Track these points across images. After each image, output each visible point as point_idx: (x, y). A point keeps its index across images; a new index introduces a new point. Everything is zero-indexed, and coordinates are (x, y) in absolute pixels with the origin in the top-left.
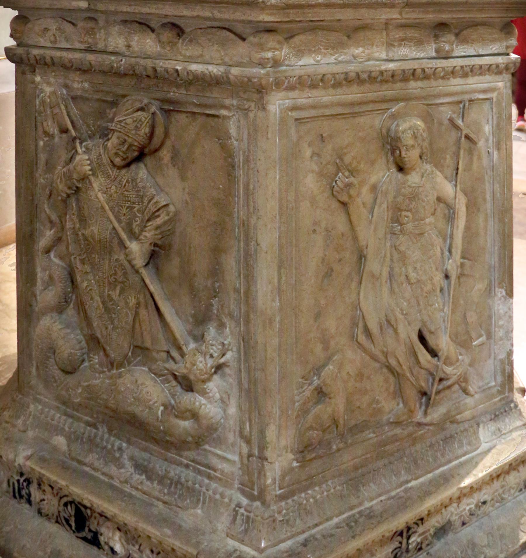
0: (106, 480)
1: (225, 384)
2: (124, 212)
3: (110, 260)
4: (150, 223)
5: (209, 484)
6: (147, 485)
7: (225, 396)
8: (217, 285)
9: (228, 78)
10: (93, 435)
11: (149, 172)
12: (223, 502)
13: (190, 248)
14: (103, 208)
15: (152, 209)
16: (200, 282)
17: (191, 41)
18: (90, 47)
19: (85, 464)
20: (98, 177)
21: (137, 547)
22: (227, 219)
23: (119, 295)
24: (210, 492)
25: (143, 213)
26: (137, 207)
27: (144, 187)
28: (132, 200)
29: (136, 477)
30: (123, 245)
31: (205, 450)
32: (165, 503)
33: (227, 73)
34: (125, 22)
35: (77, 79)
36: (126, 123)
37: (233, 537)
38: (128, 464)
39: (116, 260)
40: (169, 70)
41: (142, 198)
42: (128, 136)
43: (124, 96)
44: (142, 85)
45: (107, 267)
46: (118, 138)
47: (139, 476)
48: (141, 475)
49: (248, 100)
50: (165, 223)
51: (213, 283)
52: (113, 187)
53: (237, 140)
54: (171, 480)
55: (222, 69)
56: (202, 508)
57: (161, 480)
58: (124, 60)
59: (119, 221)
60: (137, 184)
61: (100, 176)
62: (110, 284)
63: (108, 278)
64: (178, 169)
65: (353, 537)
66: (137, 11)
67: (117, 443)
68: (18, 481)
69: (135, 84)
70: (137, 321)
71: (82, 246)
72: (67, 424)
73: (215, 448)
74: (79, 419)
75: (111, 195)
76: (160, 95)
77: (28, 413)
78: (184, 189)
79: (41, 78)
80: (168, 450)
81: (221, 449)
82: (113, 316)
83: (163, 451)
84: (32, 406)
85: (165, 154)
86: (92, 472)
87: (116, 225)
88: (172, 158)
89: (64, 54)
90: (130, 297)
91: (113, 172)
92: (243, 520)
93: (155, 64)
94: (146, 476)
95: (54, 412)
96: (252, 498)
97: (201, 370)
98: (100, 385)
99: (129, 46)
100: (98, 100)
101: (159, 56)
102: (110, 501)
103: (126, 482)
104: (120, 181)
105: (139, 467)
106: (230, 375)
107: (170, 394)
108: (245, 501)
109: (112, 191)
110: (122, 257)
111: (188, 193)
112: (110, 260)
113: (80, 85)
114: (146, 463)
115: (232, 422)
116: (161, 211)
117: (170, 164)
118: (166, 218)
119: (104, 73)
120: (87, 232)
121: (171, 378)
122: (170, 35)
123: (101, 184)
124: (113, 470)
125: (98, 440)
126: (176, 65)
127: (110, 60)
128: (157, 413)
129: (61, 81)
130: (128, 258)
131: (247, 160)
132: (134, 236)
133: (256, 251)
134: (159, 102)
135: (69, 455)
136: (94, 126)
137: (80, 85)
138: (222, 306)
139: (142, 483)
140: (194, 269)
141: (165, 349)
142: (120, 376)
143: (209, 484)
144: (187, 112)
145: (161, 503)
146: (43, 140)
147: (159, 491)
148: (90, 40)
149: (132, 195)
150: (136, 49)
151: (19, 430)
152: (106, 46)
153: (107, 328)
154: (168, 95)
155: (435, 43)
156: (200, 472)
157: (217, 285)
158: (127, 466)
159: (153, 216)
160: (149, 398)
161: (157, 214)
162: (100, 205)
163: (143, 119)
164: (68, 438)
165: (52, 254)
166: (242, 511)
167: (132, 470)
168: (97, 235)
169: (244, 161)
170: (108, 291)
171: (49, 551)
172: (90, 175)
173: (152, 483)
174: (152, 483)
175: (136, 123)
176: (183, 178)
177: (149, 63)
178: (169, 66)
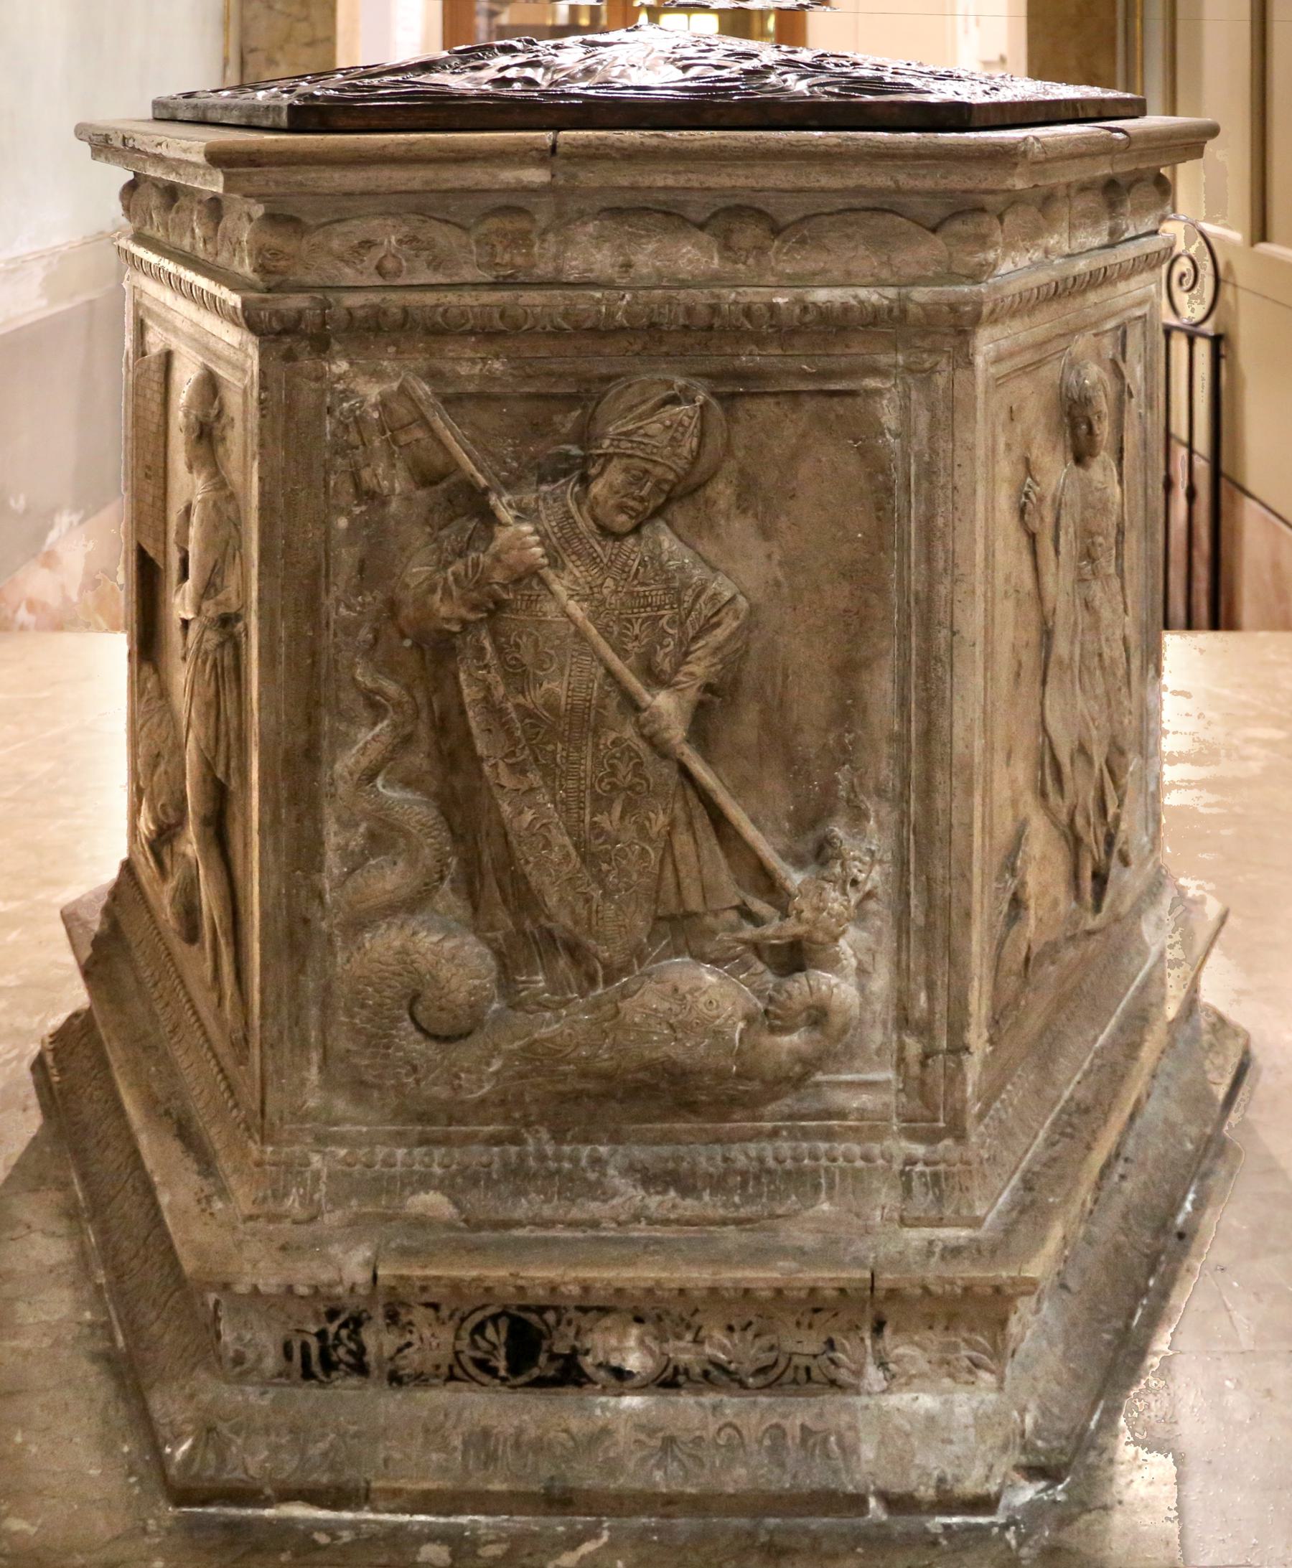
0: (579, 1235)
1: (865, 934)
2: (637, 631)
3: (596, 745)
4: (701, 643)
5: (832, 1149)
6: (689, 1207)
7: (866, 958)
8: (848, 738)
9: (904, 311)
10: (514, 1158)
11: (680, 537)
12: (876, 1169)
13: (786, 676)
14: (580, 635)
15: (705, 612)
16: (810, 742)
17: (802, 241)
18: (511, 276)
19: (519, 1224)
20: (564, 567)
21: (689, 1336)
22: (874, 599)
23: (622, 818)
24: (841, 1162)
25: (682, 624)
26: (667, 613)
27: (681, 569)
28: (656, 601)
29: (653, 1201)
30: (631, 704)
31: (818, 1085)
32: (738, 1222)
33: (903, 301)
34: (616, 212)
35: (469, 353)
36: (646, 435)
37: (917, 1223)
38: (619, 1182)
39: (613, 743)
40: (755, 307)
41: (679, 592)
42: (655, 462)
43: (607, 379)
44: (664, 349)
45: (589, 763)
46: (626, 470)
47: (658, 1198)
48: (664, 1192)
49: (931, 351)
50: (733, 635)
51: (841, 736)
52: (609, 582)
53: (897, 436)
54: (744, 1174)
55: (891, 292)
56: (830, 1198)
57: (718, 1184)
58: (628, 297)
59: (622, 653)
60: (662, 565)
61: (571, 565)
62: (597, 798)
63: (592, 786)
64: (756, 515)
65: (1089, 1148)
66: (696, 185)
67: (585, 1151)
68: (321, 1335)
69: (644, 348)
70: (669, 860)
71: (518, 733)
72: (437, 1161)
73: (838, 1072)
74: (468, 1139)
75: (603, 602)
76: (715, 364)
77: (308, 1175)
78: (769, 556)
79: (351, 364)
80: (725, 1118)
81: (851, 1070)
82: (605, 867)
83: (708, 1126)
84: (316, 1159)
85: (722, 492)
86: (541, 1233)
87: (617, 664)
88: (739, 496)
89: (430, 298)
90: (652, 815)
91: (603, 548)
92: (926, 1184)
93: (718, 297)
94: (677, 1190)
95: (386, 1150)
96: (932, 1137)
97: (840, 915)
98: (567, 1031)
99: (627, 266)
100: (529, 397)
101: (715, 279)
102: (630, 1263)
103: (636, 1218)
104: (625, 564)
105: (650, 1179)
106: (875, 914)
107: (754, 991)
108: (919, 1150)
109: (605, 591)
110: (629, 732)
111: (780, 564)
112: (596, 745)
113: (479, 367)
114: (671, 1165)
115: (878, 1007)
116: (723, 614)
117: (734, 511)
118: (735, 624)
119: (558, 332)
120: (534, 698)
121: (751, 957)
122: (758, 231)
123: (576, 581)
124: (595, 1208)
125: (532, 1162)
126: (773, 295)
127: (592, 297)
128: (732, 1040)
129: (421, 362)
130: (646, 731)
131: (929, 472)
132: (655, 679)
133: (951, 648)
134: (706, 382)
135: (466, 1221)
136: (517, 459)
137: (479, 367)
138: (860, 777)
139: (674, 1206)
140: (795, 718)
141: (736, 902)
142: (625, 994)
143: (832, 1149)
144: (775, 394)
145: (732, 1227)
146: (350, 513)
147: (724, 1206)
148: (519, 260)
149: (656, 592)
150: (645, 271)
151: (295, 1222)
152: (559, 270)
153: (588, 900)
154: (737, 363)
155: (1111, 218)
156: (806, 1134)
157: (848, 738)
158: (622, 1189)
159: (709, 626)
160: (714, 1013)
161: (715, 620)
162: (573, 628)
163: (686, 421)
164: (447, 1186)
165: (379, 782)
166: (919, 1168)
167: (641, 1193)
168: (563, 699)
169: (917, 476)
170: (593, 815)
171: (457, 1442)
172: (542, 567)
173: (699, 1198)
174: (699, 1198)
175: (671, 433)
176: (766, 533)
177: (701, 297)
178: (757, 299)
